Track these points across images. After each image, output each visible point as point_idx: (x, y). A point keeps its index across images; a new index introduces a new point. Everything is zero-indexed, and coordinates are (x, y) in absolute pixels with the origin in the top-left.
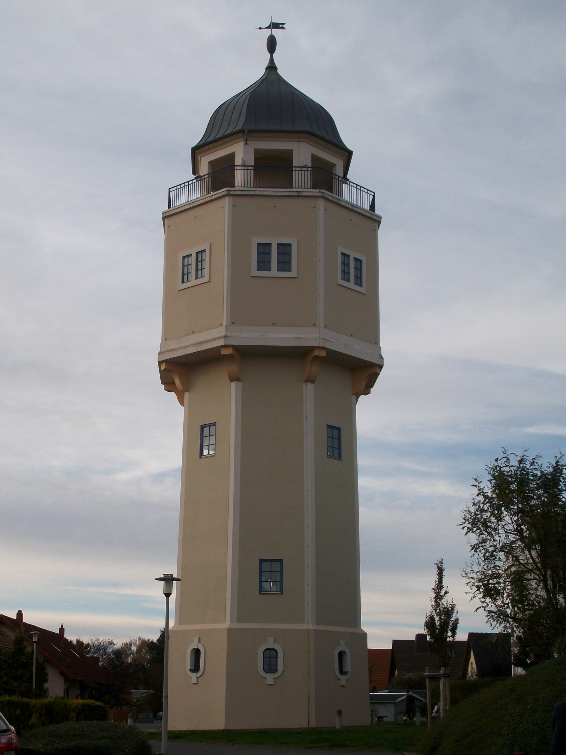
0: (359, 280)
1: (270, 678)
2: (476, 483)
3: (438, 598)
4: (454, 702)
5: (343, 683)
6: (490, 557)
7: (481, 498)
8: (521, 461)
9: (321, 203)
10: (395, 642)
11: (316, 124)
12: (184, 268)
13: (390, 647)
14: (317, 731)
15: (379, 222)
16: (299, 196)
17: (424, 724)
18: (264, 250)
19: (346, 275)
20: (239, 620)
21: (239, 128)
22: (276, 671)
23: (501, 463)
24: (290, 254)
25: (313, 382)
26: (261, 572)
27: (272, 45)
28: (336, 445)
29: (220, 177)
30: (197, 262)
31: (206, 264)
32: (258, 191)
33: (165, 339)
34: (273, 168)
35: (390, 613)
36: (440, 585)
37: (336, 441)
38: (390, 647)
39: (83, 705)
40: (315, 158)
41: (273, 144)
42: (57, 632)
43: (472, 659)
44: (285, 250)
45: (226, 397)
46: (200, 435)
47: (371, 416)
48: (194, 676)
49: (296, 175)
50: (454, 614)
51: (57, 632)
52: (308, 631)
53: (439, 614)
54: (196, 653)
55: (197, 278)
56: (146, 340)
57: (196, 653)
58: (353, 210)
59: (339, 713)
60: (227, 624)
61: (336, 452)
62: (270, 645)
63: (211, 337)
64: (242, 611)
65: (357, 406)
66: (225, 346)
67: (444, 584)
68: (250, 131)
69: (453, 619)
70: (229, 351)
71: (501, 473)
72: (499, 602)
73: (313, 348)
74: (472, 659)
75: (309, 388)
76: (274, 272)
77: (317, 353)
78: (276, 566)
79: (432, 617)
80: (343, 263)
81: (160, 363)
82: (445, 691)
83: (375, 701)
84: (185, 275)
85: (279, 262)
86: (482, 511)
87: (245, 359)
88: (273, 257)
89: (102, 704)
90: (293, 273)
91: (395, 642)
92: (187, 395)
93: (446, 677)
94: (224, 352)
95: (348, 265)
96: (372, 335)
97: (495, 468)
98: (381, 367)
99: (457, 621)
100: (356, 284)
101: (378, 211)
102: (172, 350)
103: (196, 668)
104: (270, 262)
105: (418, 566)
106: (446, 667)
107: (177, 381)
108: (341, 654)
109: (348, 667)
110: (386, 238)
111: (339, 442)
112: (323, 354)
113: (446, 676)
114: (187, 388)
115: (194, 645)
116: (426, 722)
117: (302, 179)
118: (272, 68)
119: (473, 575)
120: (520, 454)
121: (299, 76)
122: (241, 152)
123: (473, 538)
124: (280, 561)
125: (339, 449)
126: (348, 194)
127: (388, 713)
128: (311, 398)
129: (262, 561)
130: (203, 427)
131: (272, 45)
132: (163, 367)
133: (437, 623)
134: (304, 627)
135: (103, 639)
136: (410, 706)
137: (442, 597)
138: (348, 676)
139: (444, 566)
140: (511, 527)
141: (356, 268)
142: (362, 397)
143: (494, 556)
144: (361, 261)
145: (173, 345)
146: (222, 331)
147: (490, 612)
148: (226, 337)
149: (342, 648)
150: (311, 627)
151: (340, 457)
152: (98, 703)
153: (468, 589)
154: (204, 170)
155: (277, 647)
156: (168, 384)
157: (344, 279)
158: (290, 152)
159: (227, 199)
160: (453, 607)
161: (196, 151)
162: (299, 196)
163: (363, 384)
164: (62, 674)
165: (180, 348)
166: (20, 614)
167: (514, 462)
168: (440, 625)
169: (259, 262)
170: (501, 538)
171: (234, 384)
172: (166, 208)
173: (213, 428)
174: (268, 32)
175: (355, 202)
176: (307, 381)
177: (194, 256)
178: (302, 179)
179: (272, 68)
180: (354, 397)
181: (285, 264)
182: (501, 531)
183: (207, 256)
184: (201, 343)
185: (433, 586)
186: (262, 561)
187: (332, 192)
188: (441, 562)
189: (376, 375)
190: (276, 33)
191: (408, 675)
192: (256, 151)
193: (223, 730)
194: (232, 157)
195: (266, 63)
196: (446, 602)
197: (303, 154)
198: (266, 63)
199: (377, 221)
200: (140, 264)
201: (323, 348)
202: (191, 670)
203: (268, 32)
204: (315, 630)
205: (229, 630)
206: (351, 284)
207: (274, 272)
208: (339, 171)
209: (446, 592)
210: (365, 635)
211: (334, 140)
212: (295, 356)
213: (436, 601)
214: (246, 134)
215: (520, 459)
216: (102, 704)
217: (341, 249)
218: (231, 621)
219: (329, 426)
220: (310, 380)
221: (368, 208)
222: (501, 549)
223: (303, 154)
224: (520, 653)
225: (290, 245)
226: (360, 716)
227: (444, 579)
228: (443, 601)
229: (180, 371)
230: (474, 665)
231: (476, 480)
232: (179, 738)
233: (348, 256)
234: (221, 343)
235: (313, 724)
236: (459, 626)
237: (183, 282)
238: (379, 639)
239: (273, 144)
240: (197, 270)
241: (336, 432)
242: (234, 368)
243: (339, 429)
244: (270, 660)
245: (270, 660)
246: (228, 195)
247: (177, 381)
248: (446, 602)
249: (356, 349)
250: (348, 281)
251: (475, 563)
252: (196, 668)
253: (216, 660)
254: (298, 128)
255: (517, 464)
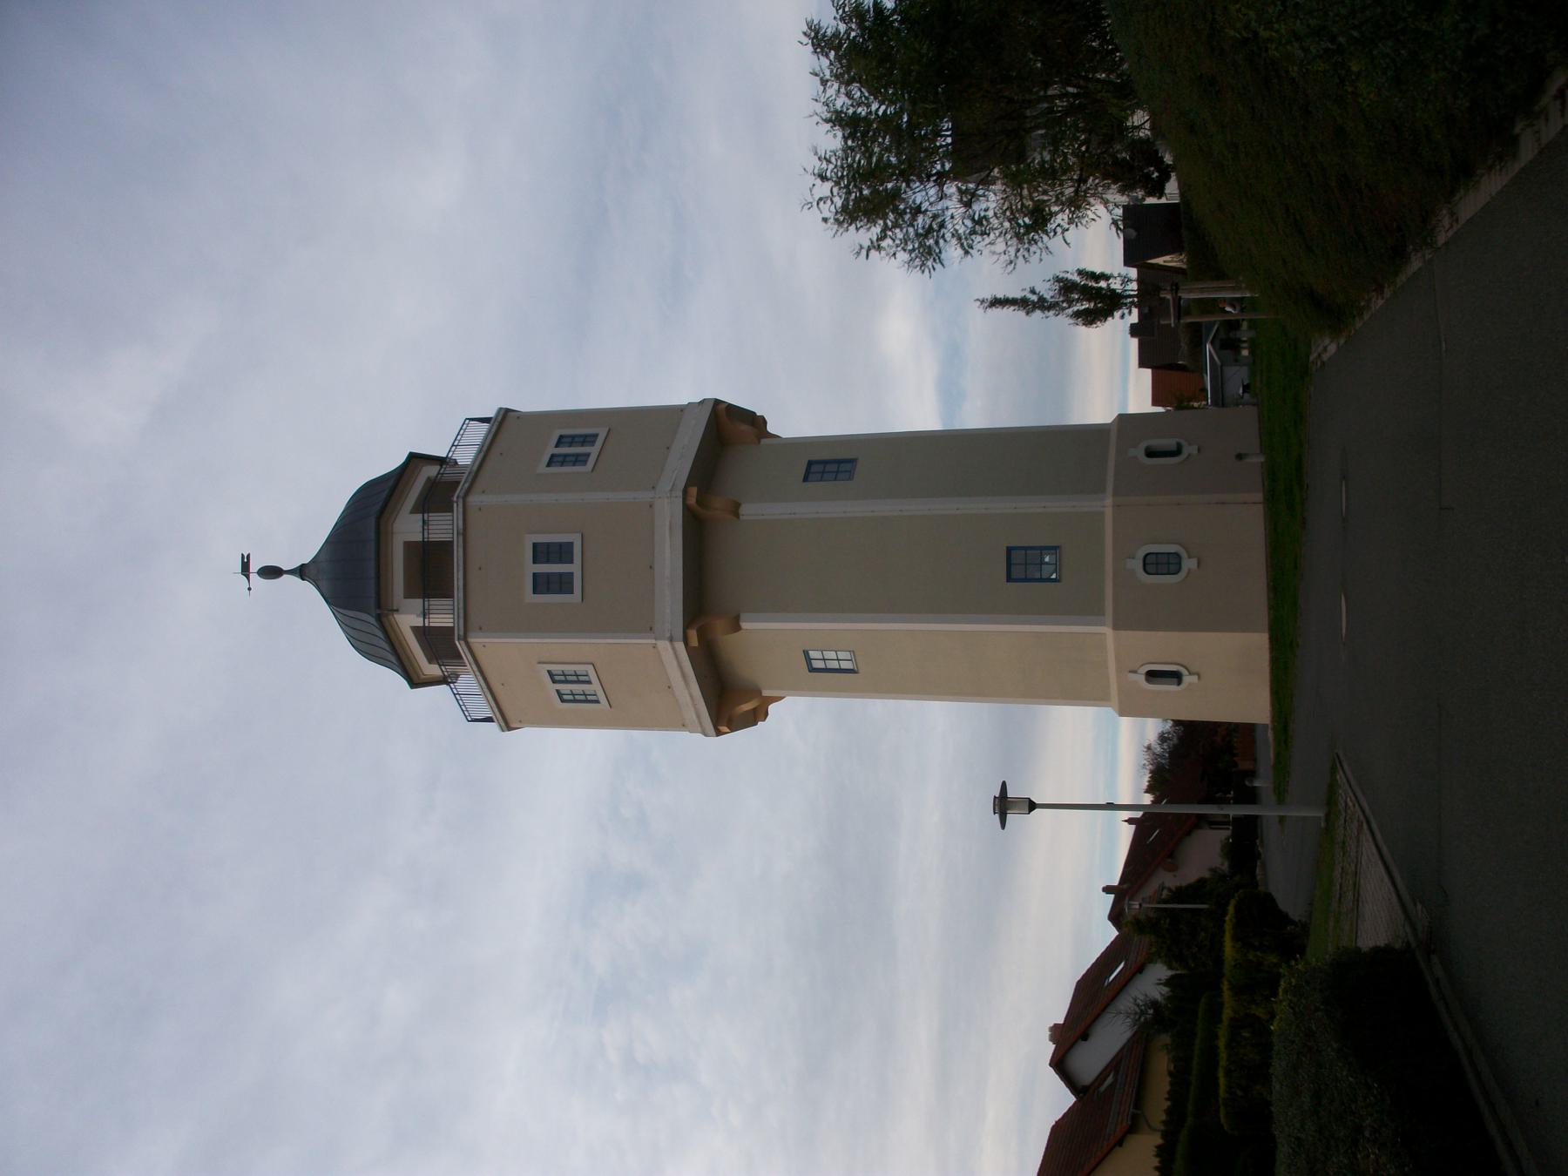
0: (588, 440)
1: (1189, 564)
2: (864, 252)
3: (1042, 305)
4: (1220, 275)
5: (1193, 450)
6: (980, 225)
7: (886, 243)
8: (823, 178)
9: (474, 499)
10: (1142, 364)
11: (374, 504)
12: (575, 699)
13: (1148, 372)
14: (1271, 499)
15: (508, 411)
16: (464, 533)
17: (1253, 325)
18: (542, 584)
19: (580, 459)
20: (1100, 612)
21: (372, 620)
22: (1177, 555)
23: (828, 210)
24: (548, 545)
25: (737, 505)
26: (1026, 580)
27: (271, 572)
28: (834, 467)
29: (441, 646)
30: (567, 682)
31: (569, 669)
32: (458, 593)
33: (683, 726)
34: (432, 571)
35: (1108, 377)
36: (1022, 303)
37: (828, 468)
38: (1148, 372)
39: (1235, 938)
40: (414, 511)
41: (407, 566)
42: (1133, 827)
43: (1160, 261)
44: (542, 553)
45: (761, 638)
46: (823, 676)
47: (795, 417)
48: (1187, 679)
49: (435, 537)
50: (1070, 276)
51: (1133, 827)
52: (1116, 506)
53: (1070, 303)
54: (1152, 676)
55: (589, 682)
56: (690, 754)
57: (1152, 676)
58: (486, 451)
59: (1240, 457)
60: (1108, 631)
61: (844, 467)
62: (1137, 565)
63: (672, 660)
64: (1087, 609)
65: (784, 435)
66: (686, 644)
67: (1018, 295)
68: (379, 606)
69: (1077, 278)
70: (693, 634)
71: (845, 208)
72: (1055, 209)
73: (686, 508)
74: (1160, 261)
75: (748, 510)
76: (575, 568)
77: (692, 501)
78: (1018, 557)
79: (1077, 315)
80: (562, 464)
81: (719, 733)
82: (1202, 290)
83: (1220, 401)
84: (587, 699)
85: (561, 561)
86: (905, 241)
87: (705, 610)
88: (553, 567)
89: (1233, 902)
90: (576, 539)
91: (1142, 364)
92: (766, 693)
93: (1177, 289)
94: (694, 642)
95: (566, 456)
96: (671, 416)
97: (840, 223)
98: (717, 402)
99: (1081, 273)
100: (593, 443)
101: (491, 414)
102: (698, 717)
103: (1176, 677)
104: (561, 575)
105: (961, 338)
106: (1159, 289)
107: (747, 707)
108: (1151, 453)
109: (1168, 443)
110: (526, 404)
111: (831, 463)
112: (694, 491)
113: (1176, 288)
114: (755, 692)
115: (1141, 678)
116: (1250, 321)
117: (442, 527)
118: (301, 572)
119: (1012, 251)
120: (812, 180)
121: (307, 529)
122: (408, 620)
123: (952, 252)
124: (1009, 550)
125: (839, 462)
126: (465, 457)
127: (1237, 377)
128: (765, 510)
129: (1009, 579)
130: (813, 670)
131: (271, 572)
132: (725, 729)
133: (1086, 305)
134: (1109, 512)
135: (1144, 759)
136: (1229, 345)
137: (1042, 299)
138: (1183, 442)
139: (988, 296)
140: (932, 192)
141: (570, 445)
142: (770, 429)
143: (981, 219)
144: (561, 437)
145: (690, 715)
146: (664, 645)
147: (1071, 221)
148: (671, 640)
149: (1139, 453)
150: (1109, 501)
151: (852, 461)
152: (1231, 909)
153: (1034, 259)
154: (433, 670)
155: (1141, 554)
156: (757, 716)
157: (585, 462)
158: (409, 546)
159: (471, 640)
160: (1058, 280)
161: (415, 681)
162: (464, 533)
163: (744, 427)
164: (1189, 833)
165: (694, 705)
166: (1107, 890)
167: (824, 189)
168: (1089, 301)
169: (560, 591)
170: (953, 207)
171: (744, 625)
172: (493, 726)
173: (813, 654)
174: (254, 577)
175: (476, 449)
176: (737, 515)
177: (558, 686)
178: (442, 527)
179: (301, 572)
180: (764, 441)
181: (561, 552)
182: (940, 206)
183: (555, 668)
184: (684, 676)
185: (1022, 313)
186: (1009, 579)
187: (458, 483)
188: (983, 302)
189: (731, 409)
190: (254, 567)
191: (1184, 347)
192: (409, 594)
193: (1271, 639)
194: (415, 629)
195: (296, 580)
196: (1048, 291)
197: (407, 527)
198: (295, 580)
199: (505, 414)
200: (567, 770)
201: (685, 492)
202: (1179, 683)
203: (254, 577)
204: (1116, 494)
205: (1116, 627)
206: (594, 451)
207: (575, 568)
208: (432, 471)
209: (1033, 292)
210: (1123, 419)
211: (391, 483)
212: (698, 533)
213: (1049, 308)
214: (382, 612)
215: (818, 181)
216: (1233, 902)
217: (542, 468)
218: (1103, 624)
219: (805, 479)
220: (735, 510)
221: (486, 426)
222: (968, 205)
223: (407, 527)
224: (1144, 187)
225: (535, 545)
226: (1243, 424)
227: (1011, 296)
228: (1047, 296)
229: (730, 702)
230: (1167, 258)
231: (858, 253)
232: (1285, 728)
233: (553, 456)
234: (680, 646)
235: (1259, 497)
236: (1090, 269)
237: (597, 702)
238: (1135, 393)
239: (407, 566)
240: (579, 682)
241: (814, 468)
242: (719, 625)
243: (810, 463)
244: (1159, 564)
245: (1159, 564)
246: (465, 638)
247: (747, 707)
248: (1048, 291)
249: (689, 440)
250: (588, 455)
251: (992, 248)
252: (1176, 677)
253: (1163, 647)
254: (372, 535)
255: (829, 184)
